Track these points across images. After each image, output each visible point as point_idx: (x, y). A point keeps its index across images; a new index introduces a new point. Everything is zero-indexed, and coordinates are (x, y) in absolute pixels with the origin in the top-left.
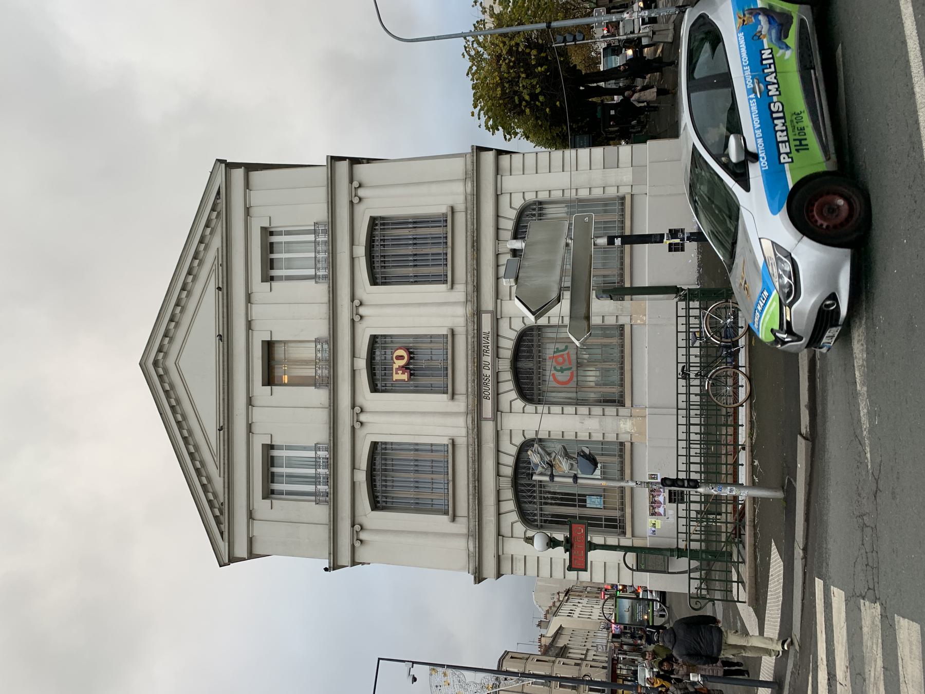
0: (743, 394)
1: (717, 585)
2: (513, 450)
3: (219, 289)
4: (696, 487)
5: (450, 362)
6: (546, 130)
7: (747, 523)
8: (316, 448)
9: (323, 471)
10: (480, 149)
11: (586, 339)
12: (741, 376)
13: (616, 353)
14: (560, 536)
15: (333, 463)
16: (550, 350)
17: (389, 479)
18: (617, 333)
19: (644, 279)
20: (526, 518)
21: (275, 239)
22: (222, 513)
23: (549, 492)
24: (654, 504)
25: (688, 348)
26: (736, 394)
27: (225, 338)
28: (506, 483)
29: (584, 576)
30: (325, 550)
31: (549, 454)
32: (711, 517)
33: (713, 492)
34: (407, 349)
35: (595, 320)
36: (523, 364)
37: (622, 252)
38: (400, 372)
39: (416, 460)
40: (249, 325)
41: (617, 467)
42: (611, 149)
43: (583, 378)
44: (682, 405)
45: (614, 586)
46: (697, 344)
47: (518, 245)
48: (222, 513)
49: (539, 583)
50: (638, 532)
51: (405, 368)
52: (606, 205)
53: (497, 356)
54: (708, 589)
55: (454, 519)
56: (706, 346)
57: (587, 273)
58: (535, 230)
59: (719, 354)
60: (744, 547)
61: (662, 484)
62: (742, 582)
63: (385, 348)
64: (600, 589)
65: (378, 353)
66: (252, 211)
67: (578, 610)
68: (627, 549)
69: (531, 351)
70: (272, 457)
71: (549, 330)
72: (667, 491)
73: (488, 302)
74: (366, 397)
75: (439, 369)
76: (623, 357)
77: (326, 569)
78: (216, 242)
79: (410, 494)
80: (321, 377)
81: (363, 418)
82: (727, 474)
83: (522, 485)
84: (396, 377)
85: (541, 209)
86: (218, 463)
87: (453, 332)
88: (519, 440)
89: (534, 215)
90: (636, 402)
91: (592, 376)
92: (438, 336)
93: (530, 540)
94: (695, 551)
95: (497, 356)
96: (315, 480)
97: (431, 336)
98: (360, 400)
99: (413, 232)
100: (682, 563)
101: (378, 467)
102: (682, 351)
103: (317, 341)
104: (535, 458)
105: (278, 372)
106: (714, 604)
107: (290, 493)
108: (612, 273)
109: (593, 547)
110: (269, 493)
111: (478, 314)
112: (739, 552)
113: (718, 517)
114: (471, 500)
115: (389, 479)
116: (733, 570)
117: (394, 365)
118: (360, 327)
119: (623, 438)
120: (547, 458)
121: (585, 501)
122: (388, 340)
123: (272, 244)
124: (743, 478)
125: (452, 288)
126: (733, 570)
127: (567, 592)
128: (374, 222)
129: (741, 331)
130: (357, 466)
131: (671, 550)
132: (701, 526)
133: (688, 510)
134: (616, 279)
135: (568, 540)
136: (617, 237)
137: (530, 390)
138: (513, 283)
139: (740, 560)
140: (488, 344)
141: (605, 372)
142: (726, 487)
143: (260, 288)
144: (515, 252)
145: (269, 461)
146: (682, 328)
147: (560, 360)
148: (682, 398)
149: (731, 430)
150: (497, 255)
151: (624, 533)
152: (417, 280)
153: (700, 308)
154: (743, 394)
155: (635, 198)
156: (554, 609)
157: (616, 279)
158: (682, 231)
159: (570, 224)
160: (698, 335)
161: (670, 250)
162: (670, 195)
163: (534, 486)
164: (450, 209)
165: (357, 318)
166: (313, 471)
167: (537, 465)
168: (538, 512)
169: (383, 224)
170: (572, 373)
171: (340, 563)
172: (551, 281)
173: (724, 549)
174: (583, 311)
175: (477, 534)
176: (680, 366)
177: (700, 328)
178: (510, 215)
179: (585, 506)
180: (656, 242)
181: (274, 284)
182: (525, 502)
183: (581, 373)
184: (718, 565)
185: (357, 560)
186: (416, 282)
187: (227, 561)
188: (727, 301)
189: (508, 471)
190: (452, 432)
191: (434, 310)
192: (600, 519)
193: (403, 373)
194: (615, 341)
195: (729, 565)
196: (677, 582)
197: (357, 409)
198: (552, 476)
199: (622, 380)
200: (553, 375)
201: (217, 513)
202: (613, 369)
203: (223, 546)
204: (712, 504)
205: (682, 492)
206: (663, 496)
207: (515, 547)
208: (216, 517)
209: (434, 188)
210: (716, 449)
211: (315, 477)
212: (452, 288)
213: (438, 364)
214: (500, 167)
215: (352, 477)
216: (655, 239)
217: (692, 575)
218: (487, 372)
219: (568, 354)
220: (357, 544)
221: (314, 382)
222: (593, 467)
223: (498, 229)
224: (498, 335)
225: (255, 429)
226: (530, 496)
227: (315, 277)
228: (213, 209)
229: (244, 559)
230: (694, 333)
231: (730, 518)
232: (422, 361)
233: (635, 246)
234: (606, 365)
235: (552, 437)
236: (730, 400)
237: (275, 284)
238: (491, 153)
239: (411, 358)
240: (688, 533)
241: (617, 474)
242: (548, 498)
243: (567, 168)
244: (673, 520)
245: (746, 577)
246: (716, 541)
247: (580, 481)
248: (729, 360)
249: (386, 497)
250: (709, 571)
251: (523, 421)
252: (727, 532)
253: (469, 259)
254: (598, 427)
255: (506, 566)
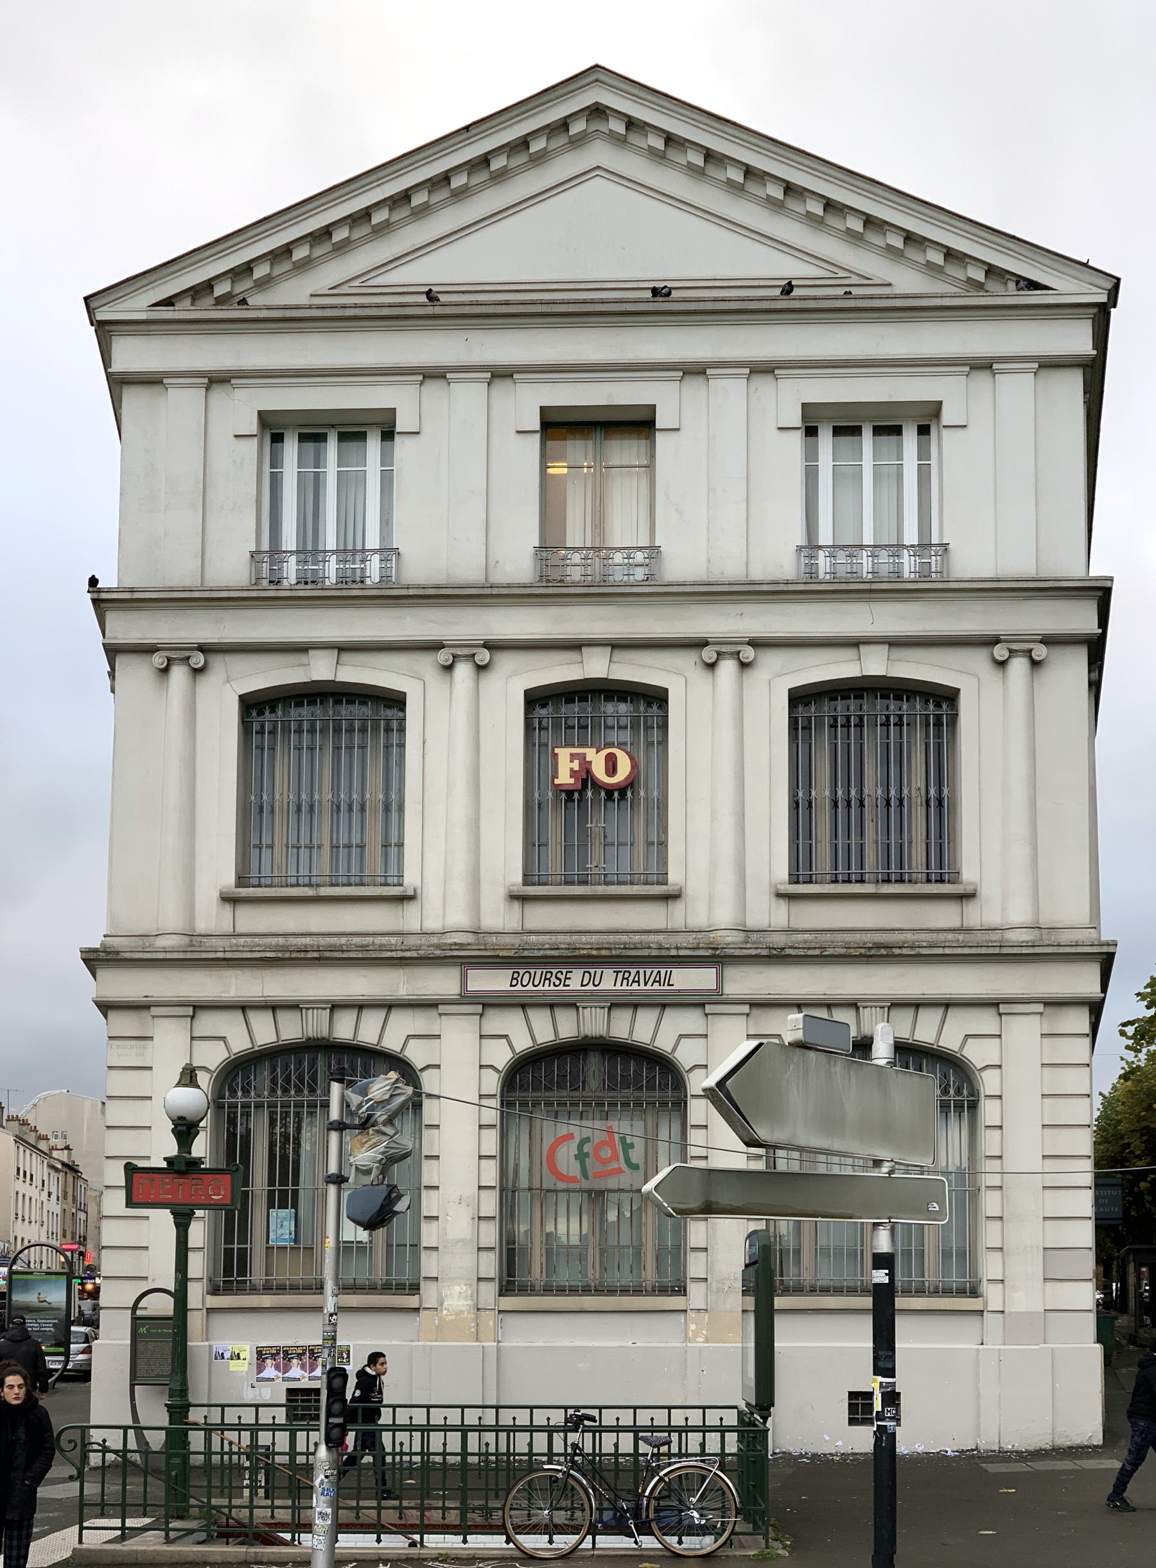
0: (533, 1542)
1: (114, 1488)
2: (392, 1043)
3: (788, 289)
4: (328, 1441)
5: (601, 890)
6: (1140, 1119)
7: (253, 1550)
8: (388, 552)
9: (331, 569)
10: (1106, 962)
11: (659, 1206)
12: (573, 1539)
13: (623, 1278)
14: (200, 1147)
15: (352, 595)
16: (626, 1126)
17: (319, 736)
18: (668, 1280)
19: (788, 1338)
20: (238, 1070)
21: (910, 438)
22: (221, 301)
23: (298, 1129)
24: (284, 1356)
25: (635, 1430)
26: (533, 1529)
27: (661, 304)
28: (315, 1025)
29: (115, 1202)
30: (140, 579)
31: (390, 1121)
32: (261, 1477)
33: (319, 1479)
34: (631, 783)
35: (697, 1231)
36: (594, 1065)
37: (852, 1291)
38: (576, 765)
39: (363, 808)
40: (695, 371)
41: (363, 1278)
42: (1088, 1264)
43: (562, 1209)
44: (506, 1417)
45: (92, 1271)
46: (644, 1448)
47: (882, 1051)
48: (221, 301)
49: (88, 1104)
50: (219, 1320)
51: (586, 778)
52: (961, 1255)
53: (616, 1004)
54: (103, 1468)
55: (230, 900)
56: (640, 1469)
57: (809, 1209)
58: (918, 1090)
59: (623, 1494)
60: (199, 1543)
61: (333, 1369)
62: (123, 1538)
63: (635, 727)
64: (83, 1241)
65: (623, 708)
66: (983, 378)
67: (32, 1191)
68: (180, 1295)
69: (625, 1085)
70: (361, 437)
71: (676, 1127)
72: (316, 1385)
73: (745, 982)
74: (516, 679)
75: (583, 861)
76: (612, 1292)
77: (93, 581)
78: (906, 281)
79: (282, 793)
80: (564, 563)
81: (463, 671)
82: (358, 1508)
83: (313, 1064)
84: (564, 754)
85: (959, 1107)
86: (345, 289)
87: (672, 897)
88: (416, 1055)
89: (945, 1091)
90: (511, 1320)
91: (569, 1227)
92: (663, 861)
93: (189, 1077)
94: (186, 1443)
95: (616, 1004)
96: (310, 551)
97: (663, 844)
98: (507, 662)
99: (918, 800)
100: (155, 1412)
101: (345, 711)
102: (626, 1419)
103: (653, 551)
104: (380, 1086)
105: (577, 449)
106: (71, 1478)
107: (276, 482)
108: (807, 1270)
109: (182, 1222)
110: (273, 428)
111: (718, 958)
112: (190, 1532)
113: (261, 1492)
114: (273, 941)
115: (319, 736)
116: (147, 1521)
117: (595, 736)
118: (686, 661)
119: (429, 1294)
120: (380, 1116)
121: (283, 1205)
122: (655, 735)
123: (897, 431)
124: (349, 1542)
125: (780, 895)
126: (147, 1521)
127: (71, 1168)
128: (945, 699)
129: (672, 1540)
130: (346, 657)
131: (183, 1392)
132: (239, 1454)
133: (274, 1428)
134: (791, 1276)
135: (194, 1165)
136: (891, 1275)
137: (534, 1082)
138: (788, 1038)
139: (172, 1535)
140: (644, 982)
141: (578, 1254)
142: (331, 1505)
143: (787, 399)
144: (864, 1046)
145: (352, 429)
146: (678, 1418)
147: (606, 1153)
148: (523, 1418)
149: (453, 1517)
150: (853, 1005)
151: (215, 1291)
152: (800, 809)
153: (723, 1454)
154: (533, 1542)
155: (975, 1320)
156: (31, 1139)
157: (790, 1277)
158: (897, 1419)
159: (922, 1170)
160: (664, 1449)
161: (852, 1395)
162: (978, 1397)
163: (312, 1090)
164: (970, 889)
165: (708, 654)
166: (331, 543)
167: (364, 1092)
168: (253, 1098)
169: (938, 723)
170: (574, 1179)
171: (110, 617)
172: (796, 1126)
173: (193, 1502)
174: (723, 1198)
175: (195, 957)
176: (595, 1413)
177: (680, 1455)
178: (947, 1034)
179: (271, 1205)
180: (875, 1358)
181: (797, 438)
182: (273, 1070)
183: (576, 1199)
184: (157, 1489)
185: (120, 660)
186: (794, 805)
187: (100, 316)
188: (738, 1513)
189: (344, 1029)
190: (432, 895)
191: (727, 848)
192: (243, 1239)
193: (573, 773)
194: (650, 1275)
195: (162, 1511)
196: (112, 1403)
197: (484, 656)
198: (340, 1127)
199: (561, 1291)
200: (570, 1136)
201: (221, 289)
202: (584, 1272)
203: (136, 306)
204: (294, 1482)
205: (317, 1417)
206: (301, 1376)
207: (170, 1046)
208: (208, 286)
209: (1020, 852)
210: (411, 1487)
211: (315, 551)
212: (780, 895)
213: (596, 859)
214: (1064, 1010)
215: (321, 645)
216: (884, 1358)
217: (131, 1433)
218: (575, 980)
219: (619, 1171)
220: (158, 660)
221: (549, 547)
222: (366, 1219)
223: (917, 1005)
224: (664, 1006)
225: (433, 389)
226: (288, 1080)
227: (811, 546)
228: (992, 271)
229: (106, 361)
230: (669, 1443)
231: (262, 1515)
232: (602, 820)
233: (871, 1317)
234: (592, 1256)
235: (426, 1133)
236: (519, 1517)
237: (796, 440)
238: (1097, 988)
239: (609, 792)
240: (223, 1427)
241: (349, 1278)
242: (285, 1126)
243: (1050, 1165)
244: (249, 1396)
245: (134, 1545)
246: (210, 1486)
247: (332, 1190)
248: (608, 1515)
249: (273, 732)
250: (146, 1471)
251: (462, 1064)
252: (230, 1507)
253: (849, 937)
254: (450, 1236)
255: (125, 1023)
